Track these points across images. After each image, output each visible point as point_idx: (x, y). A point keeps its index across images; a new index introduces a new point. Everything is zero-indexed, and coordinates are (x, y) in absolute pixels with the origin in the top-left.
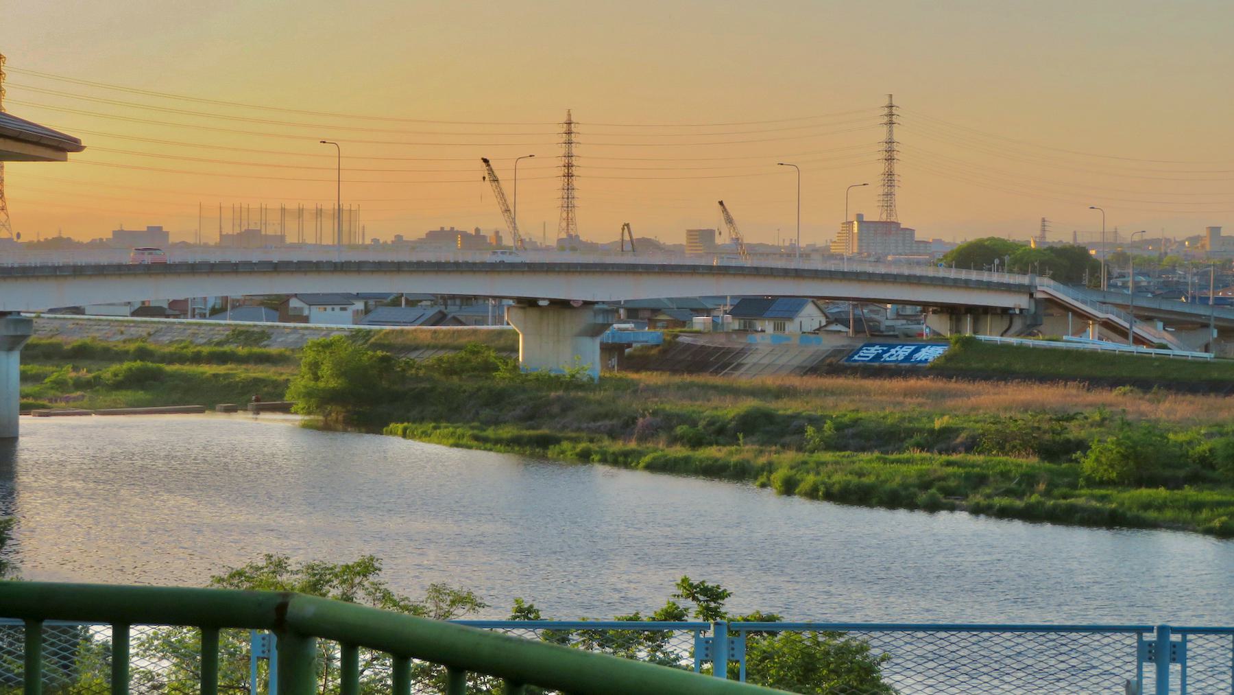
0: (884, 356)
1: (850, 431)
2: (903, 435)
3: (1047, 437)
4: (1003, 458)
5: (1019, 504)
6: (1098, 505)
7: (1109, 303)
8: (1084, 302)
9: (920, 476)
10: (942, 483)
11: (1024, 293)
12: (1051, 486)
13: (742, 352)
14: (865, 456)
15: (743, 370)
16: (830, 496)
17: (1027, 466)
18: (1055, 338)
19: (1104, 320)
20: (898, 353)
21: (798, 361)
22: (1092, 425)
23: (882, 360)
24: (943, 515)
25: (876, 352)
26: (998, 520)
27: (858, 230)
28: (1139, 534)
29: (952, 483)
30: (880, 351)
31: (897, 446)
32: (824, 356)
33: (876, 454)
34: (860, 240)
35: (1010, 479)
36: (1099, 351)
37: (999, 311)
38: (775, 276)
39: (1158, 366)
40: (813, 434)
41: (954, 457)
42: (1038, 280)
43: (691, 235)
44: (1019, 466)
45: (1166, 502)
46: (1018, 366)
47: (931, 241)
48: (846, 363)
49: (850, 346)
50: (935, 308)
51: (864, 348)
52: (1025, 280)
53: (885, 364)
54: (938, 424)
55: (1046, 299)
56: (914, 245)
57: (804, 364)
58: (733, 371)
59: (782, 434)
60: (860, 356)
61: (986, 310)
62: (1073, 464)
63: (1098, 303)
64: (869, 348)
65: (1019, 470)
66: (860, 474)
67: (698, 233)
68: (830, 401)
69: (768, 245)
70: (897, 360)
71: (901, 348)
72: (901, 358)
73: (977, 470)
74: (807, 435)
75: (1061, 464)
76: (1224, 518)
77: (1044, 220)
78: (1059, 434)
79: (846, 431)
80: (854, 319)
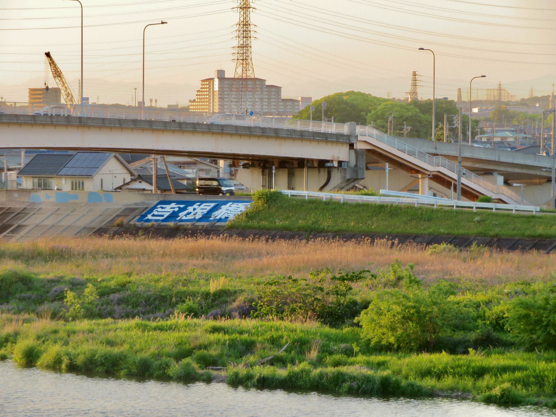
0: (180, 214)
1: (115, 297)
2: (174, 300)
3: (332, 298)
4: (278, 323)
5: (282, 373)
6: (369, 372)
7: (441, 155)
8: (411, 154)
9: (179, 344)
10: (203, 352)
11: (343, 143)
12: (325, 351)
13: (23, 213)
14: (123, 324)
15: (23, 232)
16: (73, 368)
17: (302, 331)
18: (370, 193)
19: (435, 173)
20: (195, 211)
21: (84, 222)
22: (385, 285)
23: (178, 219)
24: (199, 387)
25: (171, 210)
26: (259, 391)
27: (219, 88)
28: (383, 404)
29: (213, 352)
30: (176, 210)
31: (167, 312)
32: (114, 215)
33: (137, 320)
34: (221, 98)
35: (280, 346)
36: (416, 205)
37: (316, 165)
38: (56, 126)
39: (478, 222)
40: (73, 301)
41: (223, 323)
42: (359, 129)
43: (34, 94)
44: (293, 331)
45: (447, 367)
46: (326, 223)
47: (300, 99)
48: (138, 224)
49: (143, 203)
50: (246, 162)
51: (159, 206)
52: (345, 129)
53: (181, 223)
54: (213, 287)
55: (368, 150)
56: (281, 103)
57: (92, 225)
58: (13, 233)
59: (40, 301)
60: (153, 215)
61: (302, 163)
62: (356, 329)
63: (427, 154)
64: (164, 206)
65: (292, 335)
66: (110, 343)
67: (41, 92)
68: (89, 264)
69: (125, 106)
70: (195, 218)
71: (199, 205)
72: (198, 217)
73: (245, 336)
74: (67, 302)
75: (342, 330)
76: (506, 385)
77: (415, 74)
78: (344, 295)
79: (112, 296)
80: (157, 176)
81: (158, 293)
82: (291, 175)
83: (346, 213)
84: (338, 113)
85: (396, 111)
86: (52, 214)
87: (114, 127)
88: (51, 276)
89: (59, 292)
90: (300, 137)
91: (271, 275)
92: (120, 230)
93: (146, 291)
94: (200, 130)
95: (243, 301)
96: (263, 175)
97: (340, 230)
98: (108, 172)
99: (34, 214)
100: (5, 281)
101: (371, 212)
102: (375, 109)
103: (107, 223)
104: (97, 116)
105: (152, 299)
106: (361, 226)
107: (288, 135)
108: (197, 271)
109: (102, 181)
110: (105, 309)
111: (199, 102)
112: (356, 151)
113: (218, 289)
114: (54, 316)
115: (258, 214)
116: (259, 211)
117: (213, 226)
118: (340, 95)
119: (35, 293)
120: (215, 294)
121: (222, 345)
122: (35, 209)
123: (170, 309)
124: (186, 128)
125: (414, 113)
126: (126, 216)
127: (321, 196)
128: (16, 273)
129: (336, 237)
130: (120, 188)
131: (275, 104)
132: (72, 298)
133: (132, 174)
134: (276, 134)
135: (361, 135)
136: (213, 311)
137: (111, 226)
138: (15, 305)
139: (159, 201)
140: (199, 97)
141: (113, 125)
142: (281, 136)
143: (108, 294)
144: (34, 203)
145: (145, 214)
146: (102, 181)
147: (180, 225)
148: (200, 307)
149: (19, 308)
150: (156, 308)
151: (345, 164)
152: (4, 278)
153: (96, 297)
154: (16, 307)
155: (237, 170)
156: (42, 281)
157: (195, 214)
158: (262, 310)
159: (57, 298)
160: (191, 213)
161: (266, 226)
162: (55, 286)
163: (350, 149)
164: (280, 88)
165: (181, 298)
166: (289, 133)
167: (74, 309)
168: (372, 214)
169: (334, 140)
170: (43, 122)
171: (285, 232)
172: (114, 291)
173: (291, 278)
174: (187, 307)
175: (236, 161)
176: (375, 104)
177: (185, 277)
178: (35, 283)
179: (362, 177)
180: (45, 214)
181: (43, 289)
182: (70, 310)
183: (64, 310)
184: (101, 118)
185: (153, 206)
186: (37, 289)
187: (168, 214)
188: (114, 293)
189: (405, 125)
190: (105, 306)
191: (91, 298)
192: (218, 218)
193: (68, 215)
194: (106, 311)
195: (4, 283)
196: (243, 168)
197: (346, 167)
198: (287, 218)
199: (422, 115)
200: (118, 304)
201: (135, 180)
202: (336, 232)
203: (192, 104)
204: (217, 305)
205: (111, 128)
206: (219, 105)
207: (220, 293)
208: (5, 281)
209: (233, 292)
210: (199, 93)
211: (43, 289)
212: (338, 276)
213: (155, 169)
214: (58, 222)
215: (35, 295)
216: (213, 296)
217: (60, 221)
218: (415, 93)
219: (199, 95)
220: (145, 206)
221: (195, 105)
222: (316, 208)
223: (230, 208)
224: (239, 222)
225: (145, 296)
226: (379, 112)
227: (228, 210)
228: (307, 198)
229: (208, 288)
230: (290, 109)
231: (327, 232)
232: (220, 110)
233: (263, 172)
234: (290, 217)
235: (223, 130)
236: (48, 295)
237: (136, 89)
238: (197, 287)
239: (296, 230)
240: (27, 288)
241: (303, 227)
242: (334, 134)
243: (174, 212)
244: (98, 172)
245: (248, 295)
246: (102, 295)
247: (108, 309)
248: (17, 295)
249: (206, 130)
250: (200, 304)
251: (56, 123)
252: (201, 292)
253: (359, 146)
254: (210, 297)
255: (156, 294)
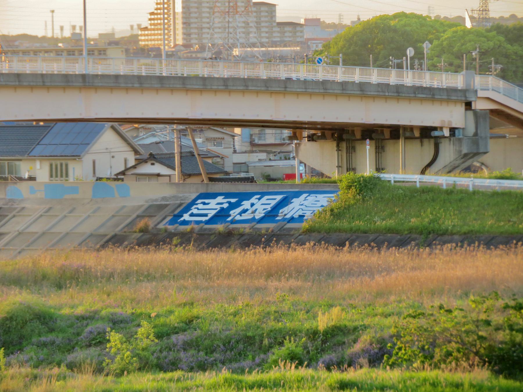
0: (231, 212)
2: (266, 342)
3: (503, 336)
11: (456, 102)
20: (254, 208)
21: (88, 228)
23: (229, 219)
25: (218, 207)
27: (183, 8)
30: (225, 206)
32: (134, 216)
37: (417, 134)
40: (119, 346)
42: (478, 81)
47: (302, 21)
48: (171, 228)
49: (175, 197)
50: (312, 132)
51: (200, 201)
55: (492, 111)
56: (276, 29)
57: (102, 231)
60: (192, 215)
64: (206, 201)
71: (259, 199)
72: (259, 215)
79: (174, 338)
81: (241, 333)
82: (379, 149)
83: (479, 205)
84: (382, 46)
85: (470, 41)
86: (41, 216)
87: (133, 88)
88: (80, 310)
89: (96, 334)
90: (396, 94)
91: (400, 302)
92: (144, 237)
93: (223, 330)
94: (253, 88)
95: (368, 341)
96: (338, 150)
97: (472, 231)
98: (105, 151)
99: (14, 216)
100: (15, 319)
101: (516, 205)
102: (438, 38)
103: (124, 228)
104: (107, 72)
105: (233, 341)
106: (503, 226)
107: (378, 91)
108: (290, 299)
109: (94, 162)
110: (166, 358)
111: (154, 30)
112: (475, 112)
113: (329, 325)
114: (99, 370)
115: (349, 210)
116: (349, 206)
117: (281, 229)
118: (384, 18)
119: (61, 336)
120: (326, 333)
121: (24, 378)
122: (15, 209)
123: (262, 356)
124: (233, 86)
125: (498, 43)
126: (150, 216)
127: (439, 182)
128: (29, 307)
129: (474, 243)
130: (123, 173)
131: (267, 30)
132: (118, 342)
133: (136, 152)
134: (362, 90)
135: (481, 90)
136: (326, 357)
137: (130, 232)
138: (32, 354)
139: (198, 194)
140: (153, 22)
141: (130, 85)
142: (369, 93)
143: (168, 335)
144: (12, 201)
145: (180, 212)
146: (94, 162)
147: (233, 229)
148: (305, 352)
149: (38, 359)
150: (240, 354)
151: (459, 132)
152: (14, 314)
153: (153, 341)
154: (34, 357)
155: (299, 144)
156: (68, 317)
157: (254, 212)
158: (400, 354)
159: (94, 342)
160: (247, 210)
161: (362, 228)
162: (87, 325)
163: (466, 109)
164: (274, 5)
165: (275, 338)
166: (379, 89)
167: (122, 359)
168: (518, 207)
169: (443, 97)
170: (32, 84)
171: (389, 235)
172: (176, 331)
173: (443, 308)
174: (288, 351)
175: (298, 131)
176: (438, 31)
177: (273, 308)
178: (58, 322)
179: (485, 151)
180: (30, 216)
181: (71, 330)
182: (116, 360)
183: (107, 361)
184: (113, 75)
185: (190, 201)
186: (62, 331)
187: (213, 212)
188: (177, 333)
189: (493, 62)
190: (165, 353)
191: (146, 342)
192: (288, 216)
193: (65, 216)
194: (167, 360)
195: (14, 323)
196: (308, 141)
197: (461, 137)
198: (391, 215)
199: (509, 46)
200: (185, 350)
201: (145, 161)
202: (465, 233)
203: (143, 32)
204: (330, 348)
205: (127, 89)
206: (184, 34)
207: (333, 331)
208: (15, 319)
209: (352, 328)
210: (153, 17)
211: (71, 330)
212: (512, 303)
213: (178, 145)
214: (50, 228)
215: (60, 339)
216: (323, 335)
217: (54, 226)
218: (486, 10)
219: (154, 19)
220: (179, 202)
221: (147, 35)
222: (433, 200)
223: (306, 203)
224: (320, 222)
225: (223, 337)
226: (445, 43)
227: (302, 205)
228: (418, 185)
229: (315, 324)
230: (290, 37)
231: (452, 234)
232: (185, 42)
233: (338, 146)
234: (395, 213)
235: (286, 87)
236: (79, 338)
237: (53, 11)
238: (297, 323)
239: (406, 232)
240: (47, 329)
241: (417, 228)
242: (443, 89)
243: (222, 209)
244: (88, 151)
245: (376, 332)
246: (159, 336)
247: (171, 357)
248: (34, 339)
249: (263, 89)
250: (305, 347)
251: (49, 84)
252: (306, 329)
253: (479, 105)
254: (319, 337)
255: (239, 335)
